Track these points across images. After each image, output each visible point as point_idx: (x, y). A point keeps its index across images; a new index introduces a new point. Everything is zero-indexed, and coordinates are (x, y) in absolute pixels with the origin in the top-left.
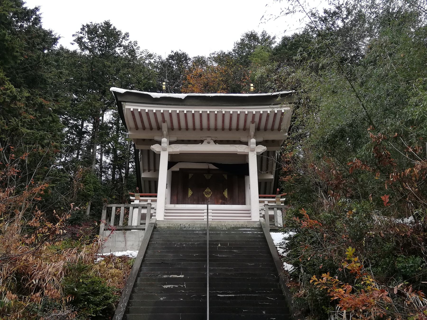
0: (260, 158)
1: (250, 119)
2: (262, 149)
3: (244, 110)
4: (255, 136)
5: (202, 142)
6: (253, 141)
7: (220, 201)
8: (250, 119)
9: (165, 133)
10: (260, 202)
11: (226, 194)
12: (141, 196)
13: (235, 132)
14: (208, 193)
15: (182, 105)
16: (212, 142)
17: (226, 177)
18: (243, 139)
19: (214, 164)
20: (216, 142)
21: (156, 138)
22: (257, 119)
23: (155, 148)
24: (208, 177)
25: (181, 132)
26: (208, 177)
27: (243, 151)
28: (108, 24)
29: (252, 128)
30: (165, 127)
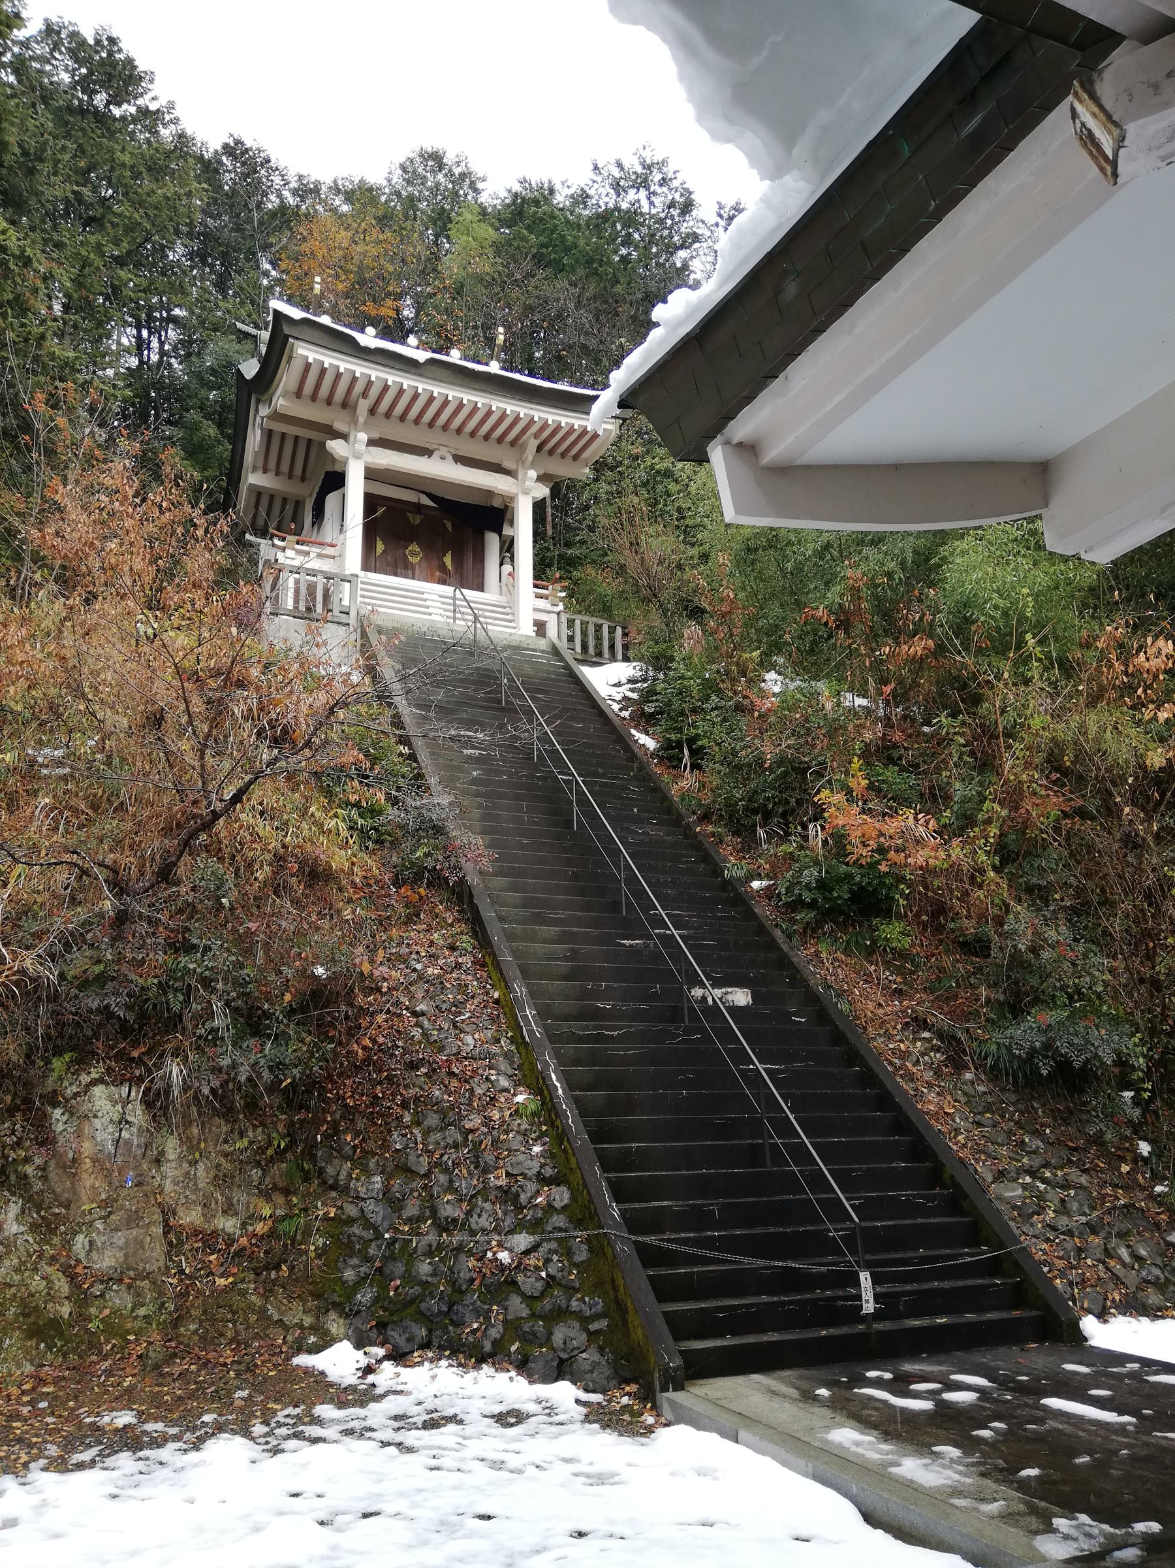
0: (539, 507)
1: (359, 388)
2: (543, 491)
3: (532, 412)
4: (366, 427)
5: (426, 452)
6: (363, 437)
7: (438, 574)
8: (359, 388)
9: (361, 420)
10: (535, 586)
11: (448, 560)
12: (298, 543)
13: (497, 445)
14: (413, 553)
15: (415, 374)
16: (450, 458)
17: (449, 526)
18: (508, 464)
19: (430, 496)
20: (459, 459)
21: (339, 426)
22: (374, 392)
23: (336, 447)
24: (416, 520)
25: (398, 423)
26: (416, 520)
27: (506, 488)
28: (665, 301)
29: (364, 406)
30: (364, 406)
